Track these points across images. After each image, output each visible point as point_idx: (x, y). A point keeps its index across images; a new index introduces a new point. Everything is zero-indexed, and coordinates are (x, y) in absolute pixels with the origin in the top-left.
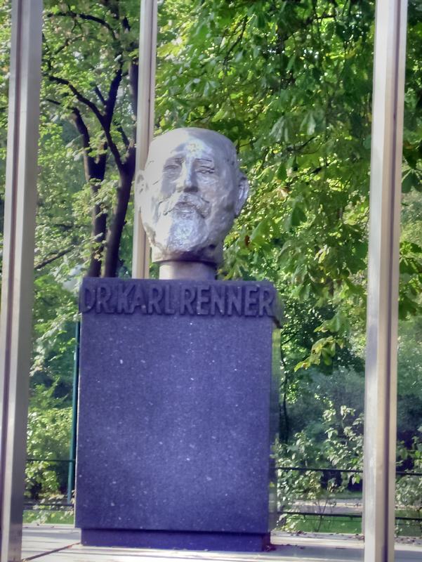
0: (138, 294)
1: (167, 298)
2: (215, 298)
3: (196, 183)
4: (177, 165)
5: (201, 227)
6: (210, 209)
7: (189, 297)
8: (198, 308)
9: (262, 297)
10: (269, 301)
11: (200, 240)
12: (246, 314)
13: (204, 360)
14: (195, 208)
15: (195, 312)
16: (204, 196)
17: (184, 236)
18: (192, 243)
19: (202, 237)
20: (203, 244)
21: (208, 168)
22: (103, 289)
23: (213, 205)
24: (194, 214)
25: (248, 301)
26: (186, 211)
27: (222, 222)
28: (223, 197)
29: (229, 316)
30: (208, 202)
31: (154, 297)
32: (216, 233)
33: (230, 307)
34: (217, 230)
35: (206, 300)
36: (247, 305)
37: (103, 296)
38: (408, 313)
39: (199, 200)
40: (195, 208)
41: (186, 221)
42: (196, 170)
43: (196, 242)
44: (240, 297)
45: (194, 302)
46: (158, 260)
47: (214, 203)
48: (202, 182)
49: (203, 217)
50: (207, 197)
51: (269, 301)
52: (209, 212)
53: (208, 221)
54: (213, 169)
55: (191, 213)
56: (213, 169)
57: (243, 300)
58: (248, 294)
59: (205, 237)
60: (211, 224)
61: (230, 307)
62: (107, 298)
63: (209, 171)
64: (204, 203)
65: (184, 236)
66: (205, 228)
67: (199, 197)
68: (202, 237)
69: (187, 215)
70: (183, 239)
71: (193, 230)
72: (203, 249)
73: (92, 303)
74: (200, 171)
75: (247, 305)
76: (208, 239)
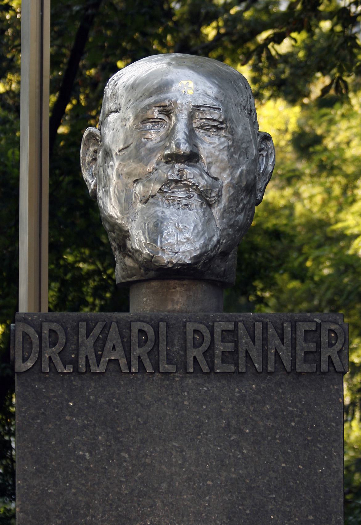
1: (163, 346)
2: (245, 340)
3: (196, 146)
4: (161, 116)
5: (208, 220)
6: (220, 190)
7: (201, 344)
8: (217, 361)
9: (324, 339)
10: (338, 346)
11: (205, 245)
12: (299, 370)
13: (186, 454)
14: (197, 189)
16: (209, 168)
17: (181, 238)
18: (195, 250)
19: (210, 239)
20: (212, 250)
21: (215, 120)
23: (226, 182)
24: (195, 202)
25: (302, 346)
26: (181, 195)
27: (238, 213)
28: (240, 170)
29: (271, 373)
30: (216, 179)
31: (195, 346)
32: (230, 231)
33: (272, 358)
34: (231, 226)
35: (230, 347)
37: (53, 344)
38: (57, 94)
39: (201, 175)
40: (197, 189)
41: (181, 211)
42: (194, 125)
43: (201, 248)
45: (209, 353)
46: (129, 280)
47: (225, 179)
48: (206, 146)
49: (210, 205)
50: (214, 171)
51: (338, 346)
52: (219, 196)
53: (216, 211)
54: (222, 123)
55: (189, 197)
56: (222, 123)
59: (215, 239)
60: (222, 217)
61: (272, 358)
63: (215, 127)
64: (210, 180)
65: (181, 238)
66: (213, 223)
67: (202, 170)
68: (210, 239)
69: (184, 202)
70: (179, 243)
71: (196, 226)
72: (211, 259)
74: (201, 127)
76: (218, 241)
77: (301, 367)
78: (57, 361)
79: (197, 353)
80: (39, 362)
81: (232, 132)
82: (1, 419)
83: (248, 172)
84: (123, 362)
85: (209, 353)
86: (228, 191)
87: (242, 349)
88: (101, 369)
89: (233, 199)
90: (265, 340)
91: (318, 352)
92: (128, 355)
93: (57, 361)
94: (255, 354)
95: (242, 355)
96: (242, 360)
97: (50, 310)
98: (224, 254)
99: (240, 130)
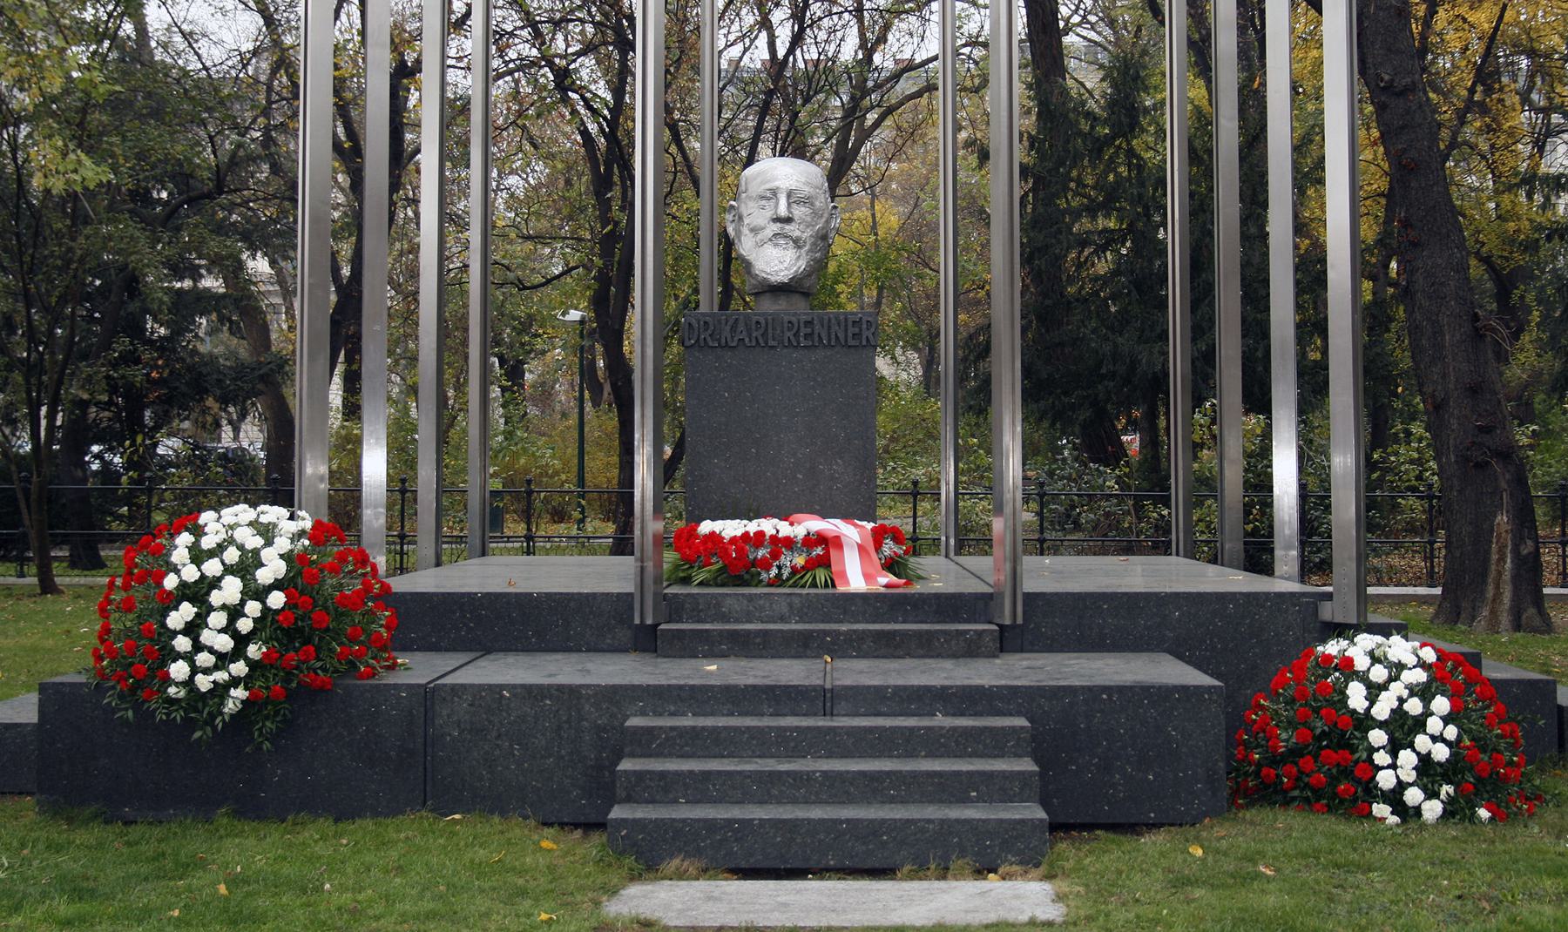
0: (741, 327)
1: (770, 331)
2: (817, 327)
9: (864, 326)
15: (766, 343)
22: (705, 323)
25: (851, 330)
33: (833, 336)
35: (809, 330)
36: (850, 335)
37: (706, 330)
44: (842, 327)
45: (796, 335)
57: (846, 330)
58: (850, 324)
61: (833, 336)
62: (710, 332)
73: (695, 337)
75: (850, 335)
77: (851, 342)
78: (709, 339)
79: (790, 334)
80: (698, 341)
81: (812, 204)
82: (1565, 390)
83: (823, 228)
84: (747, 340)
85: (796, 335)
86: (756, 294)
87: (816, 332)
88: (734, 344)
89: (814, 244)
90: (829, 327)
91: (860, 334)
92: (750, 336)
93: (709, 339)
94: (824, 335)
95: (816, 336)
96: (816, 339)
97: (622, 546)
98: (809, 275)
99: (817, 204)
